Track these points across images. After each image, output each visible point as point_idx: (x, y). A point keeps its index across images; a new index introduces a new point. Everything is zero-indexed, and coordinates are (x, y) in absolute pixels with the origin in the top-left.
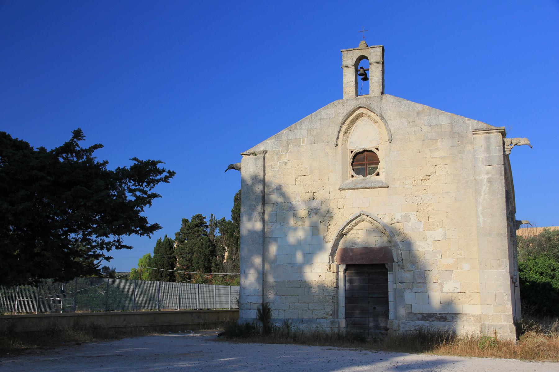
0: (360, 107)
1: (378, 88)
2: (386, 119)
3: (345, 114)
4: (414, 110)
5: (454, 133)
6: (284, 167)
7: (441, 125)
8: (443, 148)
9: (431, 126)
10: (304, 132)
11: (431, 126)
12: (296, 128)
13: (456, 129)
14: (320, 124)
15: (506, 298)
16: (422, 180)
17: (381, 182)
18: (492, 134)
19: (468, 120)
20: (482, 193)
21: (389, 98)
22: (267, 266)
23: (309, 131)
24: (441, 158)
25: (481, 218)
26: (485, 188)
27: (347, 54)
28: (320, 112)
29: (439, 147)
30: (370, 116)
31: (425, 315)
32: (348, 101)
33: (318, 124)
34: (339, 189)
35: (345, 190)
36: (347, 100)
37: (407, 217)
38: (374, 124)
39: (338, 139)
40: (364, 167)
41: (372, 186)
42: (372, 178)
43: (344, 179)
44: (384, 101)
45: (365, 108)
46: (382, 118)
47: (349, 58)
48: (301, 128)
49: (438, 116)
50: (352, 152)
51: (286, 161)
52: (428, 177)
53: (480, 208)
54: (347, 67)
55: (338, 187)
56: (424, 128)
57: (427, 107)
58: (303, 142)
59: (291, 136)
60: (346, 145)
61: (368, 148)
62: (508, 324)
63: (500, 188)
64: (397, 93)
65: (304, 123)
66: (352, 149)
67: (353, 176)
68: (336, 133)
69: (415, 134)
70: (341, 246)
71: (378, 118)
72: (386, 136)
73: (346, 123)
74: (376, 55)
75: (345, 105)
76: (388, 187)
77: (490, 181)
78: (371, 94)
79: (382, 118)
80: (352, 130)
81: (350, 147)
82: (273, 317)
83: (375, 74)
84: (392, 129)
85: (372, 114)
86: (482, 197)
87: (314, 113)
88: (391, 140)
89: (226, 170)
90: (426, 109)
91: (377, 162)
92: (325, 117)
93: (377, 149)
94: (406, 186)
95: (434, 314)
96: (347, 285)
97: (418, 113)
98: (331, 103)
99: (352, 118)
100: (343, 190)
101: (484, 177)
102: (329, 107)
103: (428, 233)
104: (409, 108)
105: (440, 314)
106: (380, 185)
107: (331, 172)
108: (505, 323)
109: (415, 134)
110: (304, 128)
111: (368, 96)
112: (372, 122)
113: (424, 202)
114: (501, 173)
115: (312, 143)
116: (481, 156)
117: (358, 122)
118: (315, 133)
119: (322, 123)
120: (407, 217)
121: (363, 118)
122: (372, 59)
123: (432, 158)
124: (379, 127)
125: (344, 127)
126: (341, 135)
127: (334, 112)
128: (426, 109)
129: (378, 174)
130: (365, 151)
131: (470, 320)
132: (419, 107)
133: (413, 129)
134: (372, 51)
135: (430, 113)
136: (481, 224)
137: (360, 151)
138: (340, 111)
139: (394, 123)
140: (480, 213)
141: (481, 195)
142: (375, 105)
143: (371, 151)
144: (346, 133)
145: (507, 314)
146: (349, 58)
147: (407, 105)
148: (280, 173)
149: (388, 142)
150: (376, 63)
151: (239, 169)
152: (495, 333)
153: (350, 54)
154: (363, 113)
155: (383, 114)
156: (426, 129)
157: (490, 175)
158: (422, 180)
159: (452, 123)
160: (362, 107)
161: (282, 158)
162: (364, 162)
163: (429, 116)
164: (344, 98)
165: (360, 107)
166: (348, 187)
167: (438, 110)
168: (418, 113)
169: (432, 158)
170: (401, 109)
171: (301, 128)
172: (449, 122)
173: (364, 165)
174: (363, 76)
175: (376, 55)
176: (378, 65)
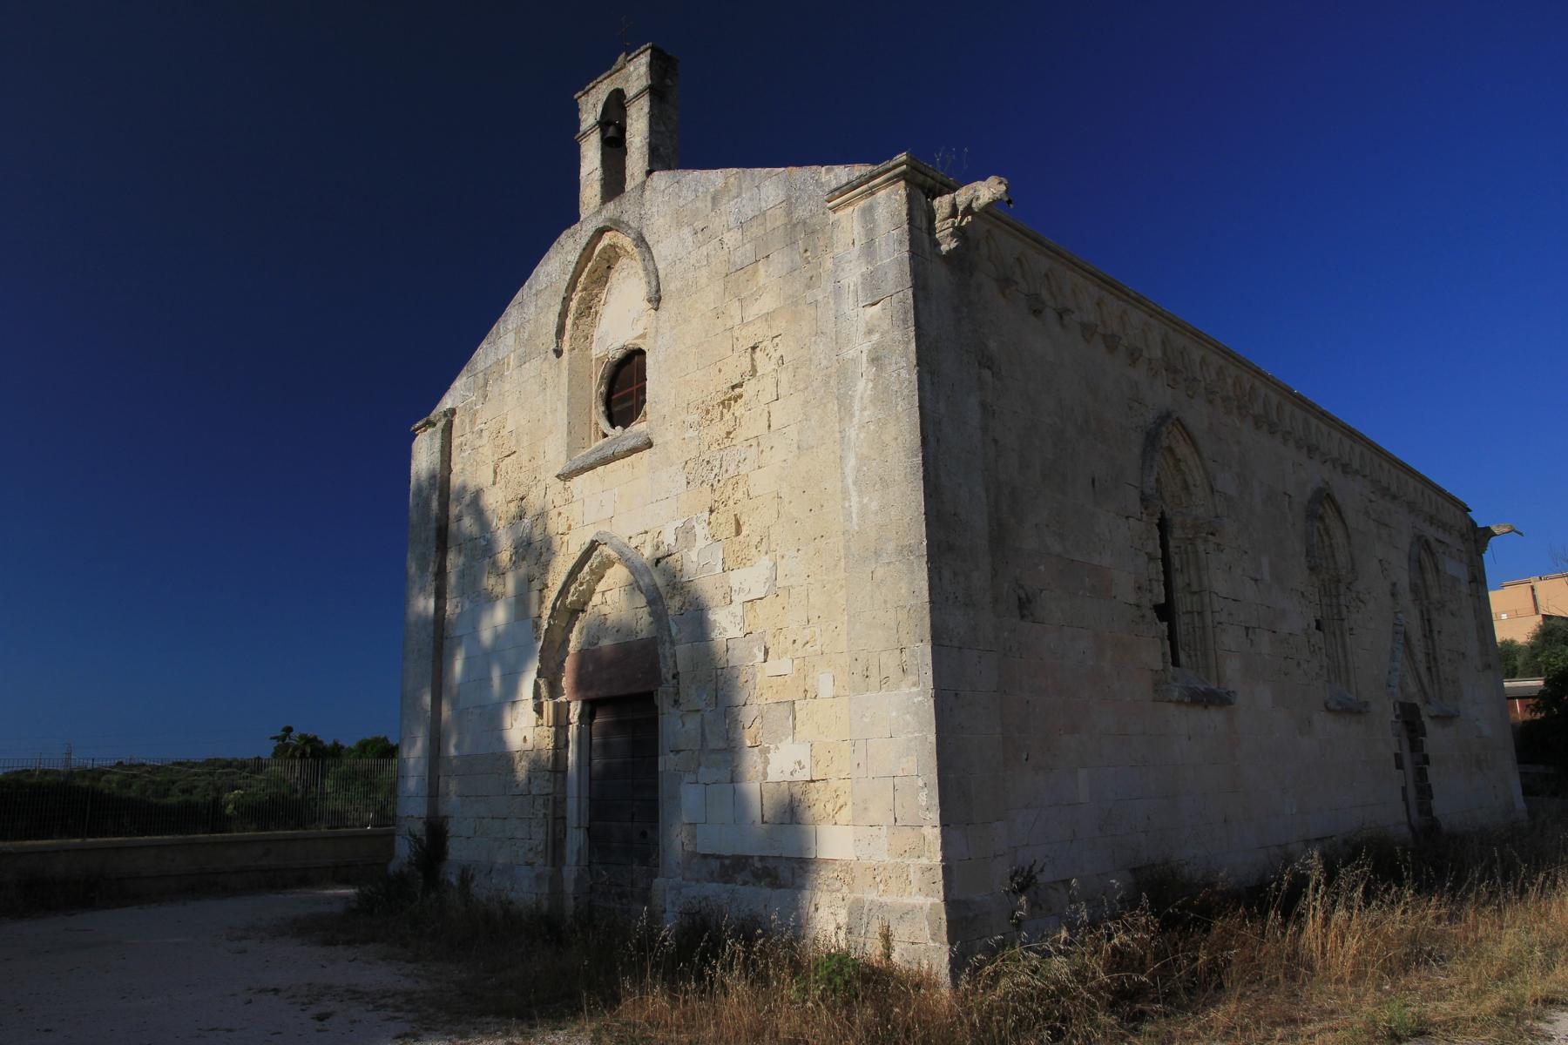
5: (795, 225)
7: (764, 213)
8: (770, 286)
15: (923, 798)
18: (882, 194)
19: (828, 172)
20: (857, 406)
21: (661, 178)
22: (446, 711)
25: (855, 499)
26: (863, 387)
31: (727, 862)
37: (686, 532)
39: (560, 332)
47: (590, 110)
52: (738, 391)
53: (852, 462)
57: (735, 170)
62: (930, 900)
63: (903, 373)
68: (553, 319)
70: (575, 641)
76: (650, 445)
77: (875, 360)
81: (596, 351)
82: (450, 857)
86: (856, 420)
95: (747, 857)
96: (595, 762)
101: (860, 347)
103: (735, 578)
104: (696, 190)
105: (762, 858)
108: (919, 900)
113: (726, 476)
114: (905, 321)
116: (853, 274)
120: (686, 532)
131: (838, 884)
136: (855, 519)
140: (850, 480)
141: (852, 416)
144: (580, 315)
145: (924, 861)
146: (590, 110)
152: (886, 937)
156: (731, 238)
157: (876, 337)
172: (782, 197)
174: (614, 144)
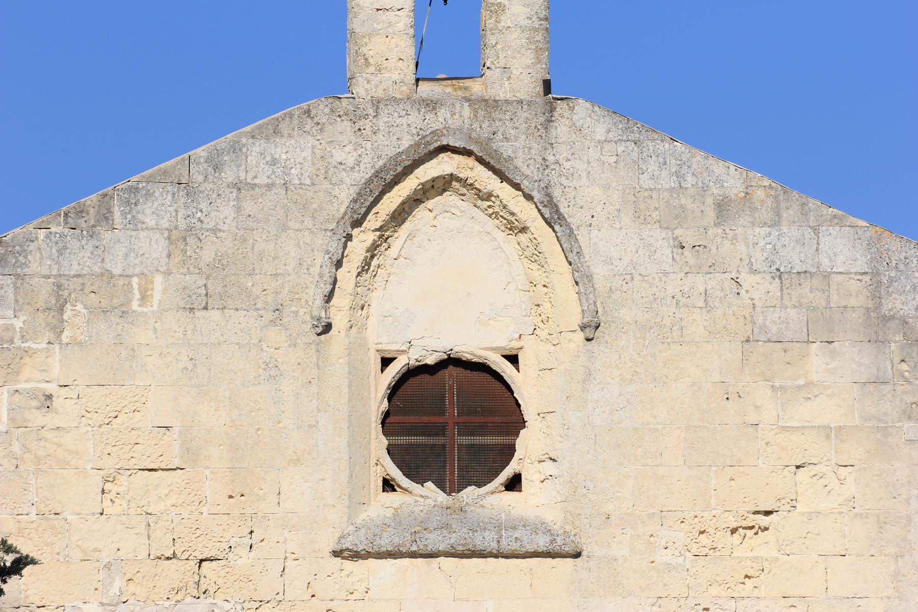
0: (444, 149)
1: (529, 58)
2: (573, 221)
3: (365, 172)
4: (705, 189)
5: (886, 319)
6: (37, 418)
7: (827, 276)
9: (779, 274)
10: (154, 247)
11: (779, 274)
12: (105, 217)
13: (895, 303)
14: (239, 209)
16: (734, 531)
17: (540, 527)
21: (585, 123)
23: (181, 238)
24: (827, 431)
28: (235, 148)
29: (814, 377)
30: (488, 196)
32: (384, 112)
33: (227, 211)
34: (337, 554)
35: (367, 555)
36: (377, 103)
38: (500, 236)
40: (438, 440)
41: (505, 546)
42: (487, 500)
43: (356, 502)
44: (561, 129)
45: (468, 153)
46: (553, 218)
48: (134, 224)
49: (815, 230)
50: (386, 362)
51: (51, 388)
55: (329, 543)
56: (748, 280)
58: (145, 298)
59: (80, 259)
60: (364, 327)
61: (470, 346)
64: (653, 103)
65: (149, 195)
66: (390, 347)
67: (388, 485)
68: (320, 262)
69: (708, 307)
71: (526, 212)
72: (569, 309)
73: (373, 222)
75: (367, 124)
76: (577, 555)
79: (553, 218)
80: (393, 252)
81: (380, 336)
84: (599, 271)
85: (504, 191)
87: (201, 152)
88: (591, 329)
89: (200, 566)
90: (760, 194)
91: (513, 421)
92: (262, 180)
93: (513, 359)
94: (663, 557)
97: (723, 207)
99: (393, 194)
100: (356, 555)
102: (284, 127)
106: (542, 543)
107: (296, 461)
109: (708, 307)
110: (150, 221)
112: (491, 224)
115: (193, 307)
117: (421, 214)
118: (207, 256)
119: (249, 207)
121: (449, 198)
123: (785, 429)
124: (536, 256)
125: (363, 238)
126: (347, 275)
127: (314, 157)
128: (760, 194)
129: (514, 483)
130: (451, 362)
132: (730, 178)
133: (699, 282)
135: (778, 213)
137: (431, 360)
138: (339, 156)
139: (610, 243)
143: (483, 368)
144: (365, 267)
147: (671, 163)
148: (16, 448)
149: (580, 336)
154: (452, 177)
155: (557, 193)
156: (758, 287)
158: (734, 531)
159: (875, 273)
161: (26, 372)
162: (450, 420)
164: (360, 89)
165: (444, 149)
166: (385, 543)
167: (813, 203)
168: (723, 207)
169: (785, 429)
171: (134, 224)
172: (862, 264)
173: (440, 430)
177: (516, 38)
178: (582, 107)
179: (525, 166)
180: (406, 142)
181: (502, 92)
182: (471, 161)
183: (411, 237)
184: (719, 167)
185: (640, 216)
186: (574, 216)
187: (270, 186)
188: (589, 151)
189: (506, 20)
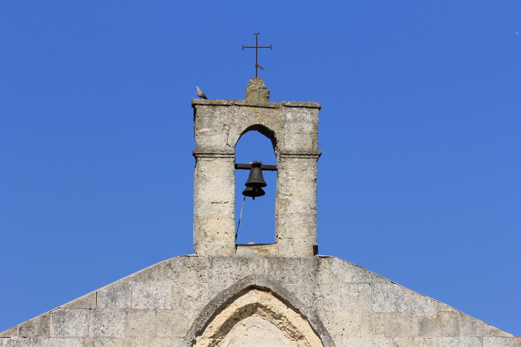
1: (304, 232)
4: (412, 313)
12: (44, 330)
14: (126, 324)
21: (338, 272)
27: (212, 116)
28: (125, 287)
30: (279, 317)
33: (120, 326)
36: (211, 260)
44: (324, 276)
47: (220, 131)
49: (480, 339)
54: (212, 155)
57: (450, 309)
64: (379, 260)
71: (303, 327)
73: (209, 332)
74: (301, 131)
75: (205, 272)
78: (283, 248)
79: (320, 330)
83: (296, 188)
87: (104, 290)
90: (446, 316)
92: (141, 307)
98: (162, 264)
102: (155, 274)
110: (72, 332)
111: (272, 250)
117: (238, 327)
119: (132, 323)
121: (255, 318)
122: (290, 141)
128: (446, 316)
132: (428, 307)
134: (289, 116)
138: (188, 291)
142: (297, 286)
146: (220, 131)
147: (391, 297)
150: (300, 155)
151: (237, 167)
153: (221, 116)
154: (258, 305)
155: (321, 315)
160: (259, 289)
163: (456, 334)
164: (202, 251)
165: (253, 287)
167: (479, 322)
168: (423, 324)
170: (376, 308)
171: (62, 334)
175: (301, 131)
176: (306, 162)
177: (297, 220)
178: (337, 262)
179: (302, 299)
180: (230, 283)
181: (288, 253)
182: (269, 295)
183: (232, 341)
184: (421, 300)
185: (373, 330)
186: (332, 329)
187: (146, 311)
188: (344, 293)
189: (290, 209)
